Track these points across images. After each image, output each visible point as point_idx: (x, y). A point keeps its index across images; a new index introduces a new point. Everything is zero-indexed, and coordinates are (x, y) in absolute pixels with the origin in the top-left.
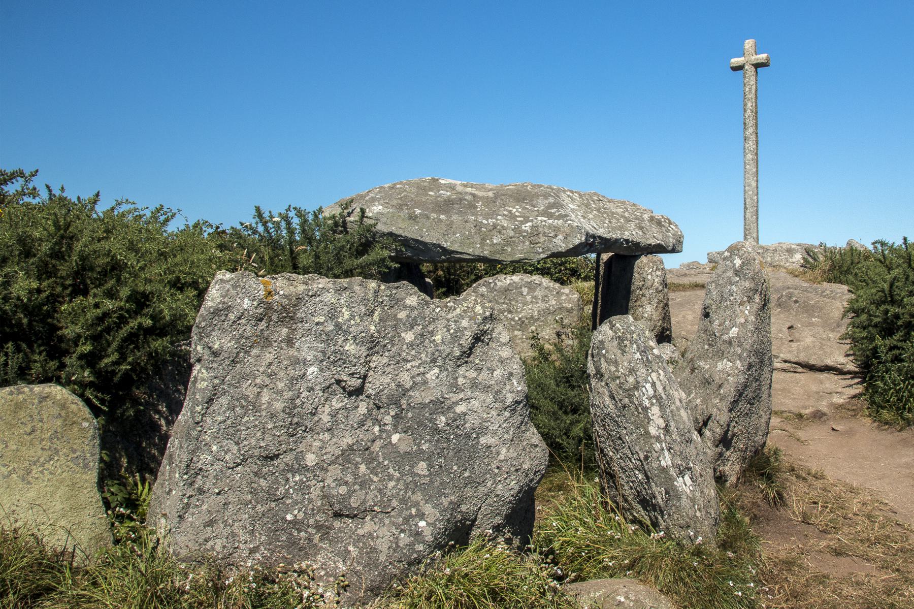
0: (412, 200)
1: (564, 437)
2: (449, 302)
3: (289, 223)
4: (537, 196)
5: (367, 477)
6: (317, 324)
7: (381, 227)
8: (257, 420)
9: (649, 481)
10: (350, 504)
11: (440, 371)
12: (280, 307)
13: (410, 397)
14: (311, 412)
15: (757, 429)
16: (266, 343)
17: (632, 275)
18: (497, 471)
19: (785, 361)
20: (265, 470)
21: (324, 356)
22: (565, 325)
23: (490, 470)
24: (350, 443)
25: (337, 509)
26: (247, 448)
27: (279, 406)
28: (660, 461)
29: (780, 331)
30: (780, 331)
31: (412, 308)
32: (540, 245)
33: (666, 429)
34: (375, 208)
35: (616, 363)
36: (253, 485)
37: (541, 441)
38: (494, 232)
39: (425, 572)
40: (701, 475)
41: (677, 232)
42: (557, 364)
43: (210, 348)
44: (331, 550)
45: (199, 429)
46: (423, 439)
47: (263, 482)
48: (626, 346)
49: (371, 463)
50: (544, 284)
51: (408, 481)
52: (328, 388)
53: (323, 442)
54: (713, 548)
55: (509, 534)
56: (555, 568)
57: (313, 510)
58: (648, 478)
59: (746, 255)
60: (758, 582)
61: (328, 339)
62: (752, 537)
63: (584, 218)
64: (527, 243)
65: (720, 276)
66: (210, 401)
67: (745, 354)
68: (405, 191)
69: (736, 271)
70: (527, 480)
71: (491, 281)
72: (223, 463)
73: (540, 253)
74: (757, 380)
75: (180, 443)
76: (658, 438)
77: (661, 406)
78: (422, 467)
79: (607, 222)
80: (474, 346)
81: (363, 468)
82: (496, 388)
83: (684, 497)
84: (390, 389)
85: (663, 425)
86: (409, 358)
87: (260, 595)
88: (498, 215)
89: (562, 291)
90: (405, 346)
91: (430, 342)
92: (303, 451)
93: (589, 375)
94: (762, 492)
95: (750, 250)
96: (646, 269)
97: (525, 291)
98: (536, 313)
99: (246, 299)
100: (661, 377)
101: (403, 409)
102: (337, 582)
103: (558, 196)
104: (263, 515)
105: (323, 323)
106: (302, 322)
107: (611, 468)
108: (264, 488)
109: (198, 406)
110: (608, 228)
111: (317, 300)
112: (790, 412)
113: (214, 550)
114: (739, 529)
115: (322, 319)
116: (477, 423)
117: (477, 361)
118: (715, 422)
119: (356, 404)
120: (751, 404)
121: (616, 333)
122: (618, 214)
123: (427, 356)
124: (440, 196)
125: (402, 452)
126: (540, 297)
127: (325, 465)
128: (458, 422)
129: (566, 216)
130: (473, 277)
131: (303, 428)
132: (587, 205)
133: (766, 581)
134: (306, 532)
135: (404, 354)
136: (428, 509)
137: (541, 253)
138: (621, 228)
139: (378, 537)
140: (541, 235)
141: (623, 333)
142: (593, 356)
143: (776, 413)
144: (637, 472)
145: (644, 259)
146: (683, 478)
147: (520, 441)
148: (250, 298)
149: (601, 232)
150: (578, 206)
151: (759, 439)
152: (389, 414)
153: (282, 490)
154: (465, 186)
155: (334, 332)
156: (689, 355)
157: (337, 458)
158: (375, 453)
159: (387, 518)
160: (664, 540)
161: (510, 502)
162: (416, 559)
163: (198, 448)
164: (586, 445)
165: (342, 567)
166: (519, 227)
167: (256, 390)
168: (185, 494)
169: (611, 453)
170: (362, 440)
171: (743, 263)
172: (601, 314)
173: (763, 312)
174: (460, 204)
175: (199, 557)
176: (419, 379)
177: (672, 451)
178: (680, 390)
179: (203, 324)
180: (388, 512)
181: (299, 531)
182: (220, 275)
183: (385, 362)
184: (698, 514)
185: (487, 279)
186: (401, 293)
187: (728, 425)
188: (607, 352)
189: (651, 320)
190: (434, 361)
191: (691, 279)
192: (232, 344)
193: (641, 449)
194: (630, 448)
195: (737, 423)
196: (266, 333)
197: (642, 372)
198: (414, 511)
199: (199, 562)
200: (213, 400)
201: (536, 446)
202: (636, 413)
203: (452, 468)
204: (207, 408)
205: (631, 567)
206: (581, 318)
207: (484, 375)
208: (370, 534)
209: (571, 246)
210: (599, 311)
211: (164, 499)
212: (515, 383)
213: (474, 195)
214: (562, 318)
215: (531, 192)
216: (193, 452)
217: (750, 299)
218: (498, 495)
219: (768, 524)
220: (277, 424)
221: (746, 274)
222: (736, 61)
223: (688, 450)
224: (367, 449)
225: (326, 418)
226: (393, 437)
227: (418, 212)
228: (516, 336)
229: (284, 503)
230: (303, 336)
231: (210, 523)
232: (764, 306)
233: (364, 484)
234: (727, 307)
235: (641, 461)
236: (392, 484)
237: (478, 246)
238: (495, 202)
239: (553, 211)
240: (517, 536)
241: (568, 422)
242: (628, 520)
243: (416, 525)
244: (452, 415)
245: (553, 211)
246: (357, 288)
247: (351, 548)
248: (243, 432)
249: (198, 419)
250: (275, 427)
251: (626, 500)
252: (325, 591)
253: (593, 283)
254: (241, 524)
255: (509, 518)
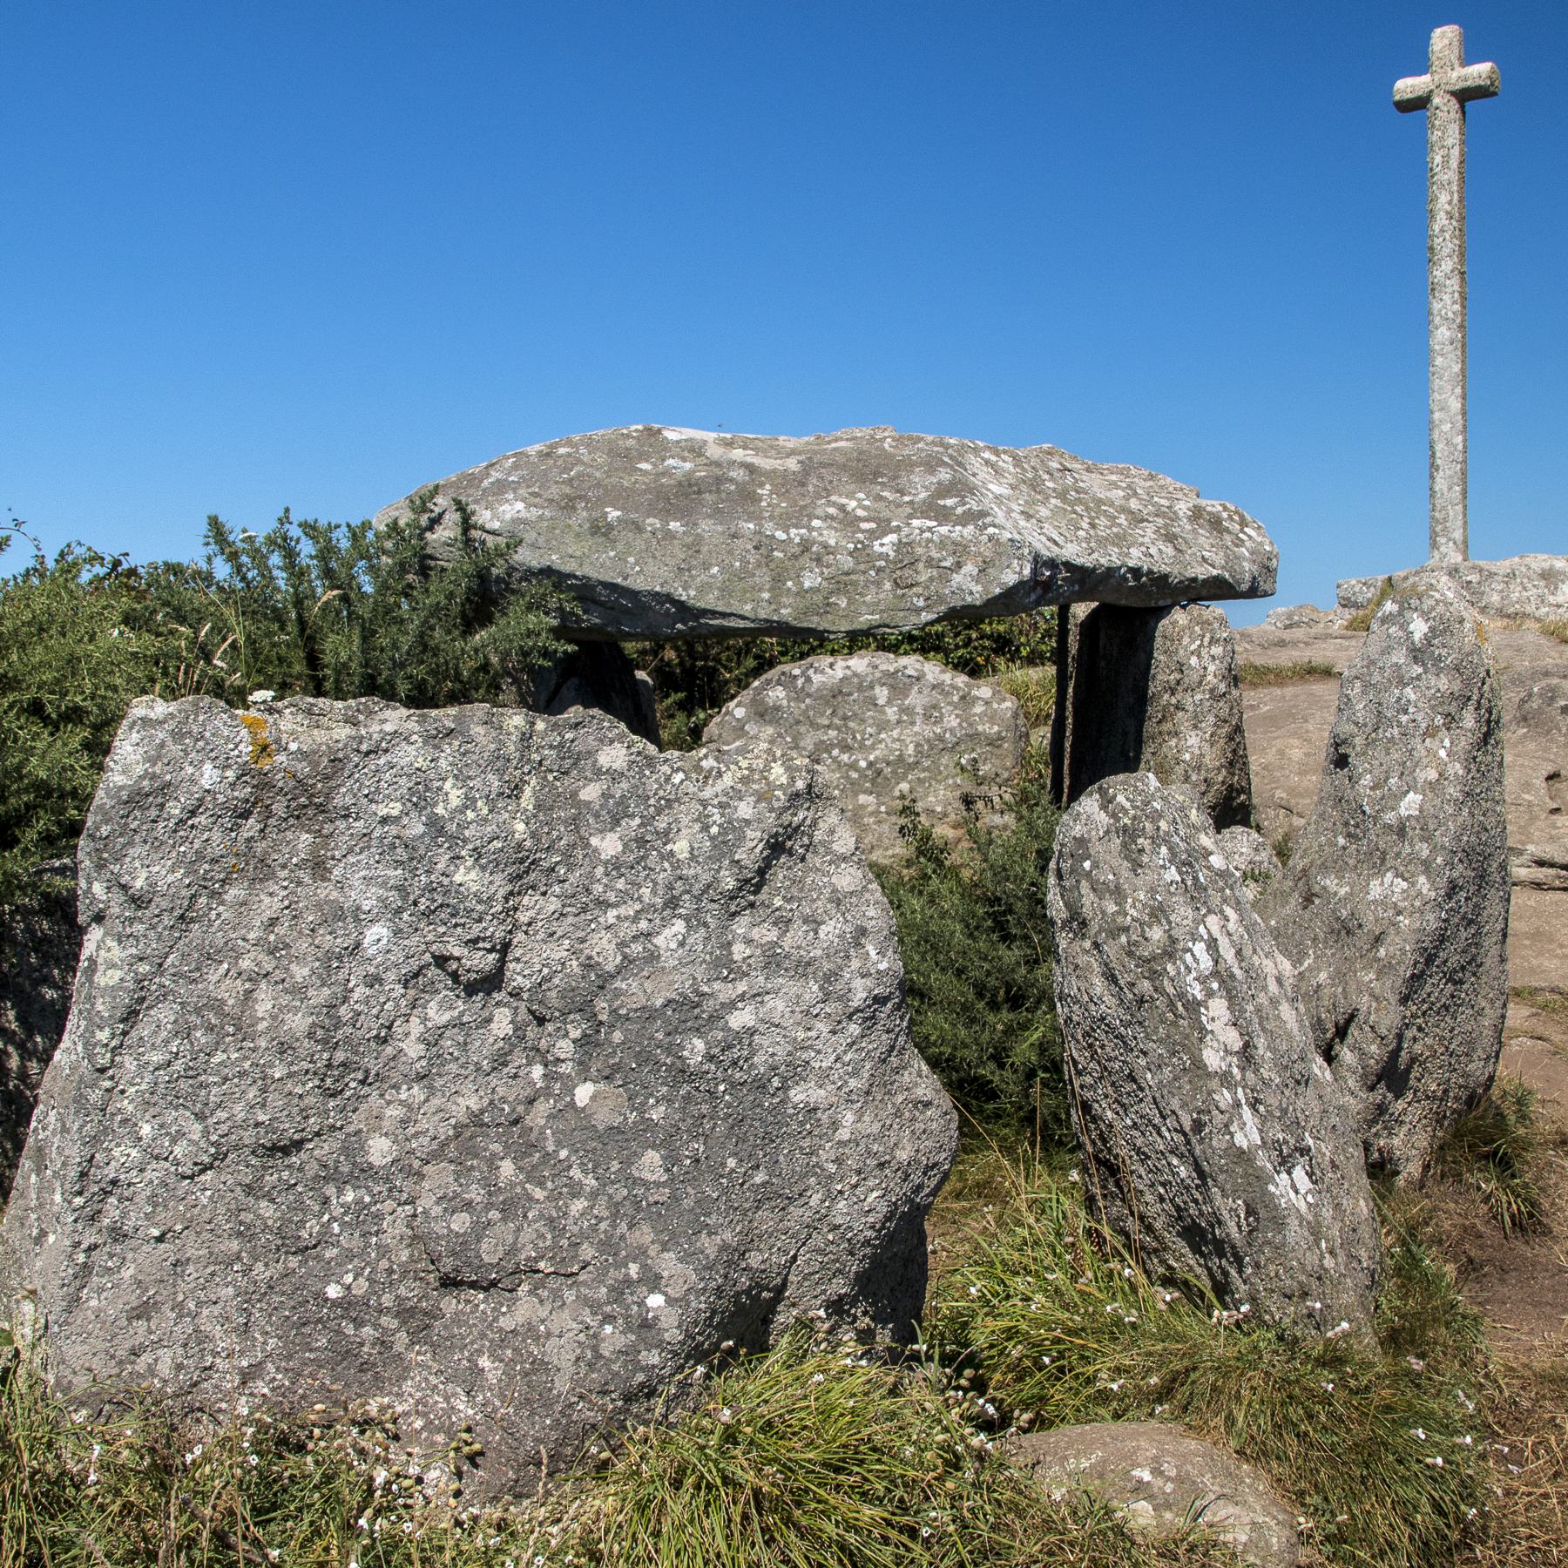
0: (598, 485)
1: (992, 1065)
2: (706, 756)
3: (290, 555)
4: (908, 465)
5: (518, 1189)
6: (384, 820)
7: (525, 557)
8: (246, 1058)
9: (1205, 1184)
10: (479, 1257)
11: (689, 927)
12: (292, 783)
13: (618, 993)
14: (377, 1037)
15: (1471, 1044)
16: (262, 871)
17: (1150, 656)
18: (832, 1168)
19: (1541, 863)
20: (270, 1179)
21: (405, 898)
22: (984, 778)
23: (817, 1165)
24: (475, 1108)
25: (448, 1268)
26: (224, 1128)
27: (298, 1023)
28: (1232, 1135)
29: (1527, 786)
30: (1527, 786)
31: (615, 776)
32: (919, 590)
33: (1246, 1054)
34: (506, 507)
35: (1118, 893)
36: (243, 1216)
37: (937, 1091)
38: (805, 560)
39: (666, 1416)
40: (1334, 1166)
41: (1261, 544)
42: (966, 874)
43: (124, 888)
44: (436, 1367)
45: (108, 1084)
46: (651, 1095)
47: (266, 1209)
48: (1141, 851)
49: (526, 1154)
50: (930, 677)
51: (618, 1198)
52: (416, 975)
53: (409, 1107)
54: (1367, 1344)
55: (867, 1320)
56: (981, 1401)
57: (390, 1271)
58: (1202, 1175)
59: (1440, 609)
60: (1485, 1431)
61: (411, 856)
62: (1464, 1317)
63: (1028, 516)
64: (888, 586)
65: (1373, 662)
66: (131, 1016)
67: (1439, 860)
68: (579, 461)
69: (1414, 650)
70: (907, 1187)
71: (797, 672)
72: (167, 1165)
73: (918, 611)
74: (1471, 922)
75: (61, 1119)
76: (1225, 1078)
77: (1231, 998)
78: (651, 1164)
79: (1085, 526)
80: (768, 866)
81: (507, 1168)
82: (827, 966)
83: (1293, 1222)
84: (566, 975)
85: (1237, 1044)
86: (612, 898)
87: (266, 1480)
88: (811, 517)
89: (975, 692)
90: (600, 870)
91: (662, 857)
92: (360, 1131)
93: (1052, 923)
94: (1487, 1199)
95: (1450, 595)
96: (1186, 640)
97: (882, 694)
98: (911, 749)
99: (208, 766)
100: (1231, 926)
101: (601, 1023)
102: (454, 1444)
103: (960, 464)
104: (271, 1288)
105: (398, 818)
106: (346, 817)
107: (1110, 1150)
108: (270, 1222)
109: (101, 1028)
110: (1087, 539)
111: (382, 761)
112: (1552, 991)
113: (154, 1376)
114: (1430, 1298)
115: (395, 809)
116: (781, 1052)
117: (778, 902)
118: (1367, 1029)
119: (485, 1014)
120: (1455, 983)
121: (1118, 819)
122: (1112, 505)
123: (654, 892)
124: (667, 473)
125: (600, 1128)
126: (919, 710)
127: (416, 1164)
128: (735, 1052)
129: (983, 514)
130: (750, 663)
131: (360, 1076)
132: (1035, 485)
133: (1503, 1426)
134: (376, 1326)
135: (598, 889)
136: (668, 1263)
137: (922, 609)
138: (1120, 540)
139: (549, 1335)
140: (921, 566)
141: (1134, 818)
142: (1060, 876)
143: (1518, 994)
144: (1175, 1162)
145: (1179, 617)
146: (1289, 1173)
147: (889, 1092)
148: (217, 763)
149: (1072, 552)
150: (1013, 487)
151: (1476, 1068)
152: (566, 1035)
153: (313, 1227)
154: (729, 444)
155: (427, 840)
156: (1296, 861)
157: (443, 1145)
158: (536, 1131)
159: (570, 1287)
160: (1245, 1327)
161: (867, 1243)
162: (642, 1385)
163: (105, 1131)
164: (1044, 1084)
165: (464, 1409)
166: (865, 547)
167: (241, 986)
168: (79, 1243)
169: (1109, 1114)
170: (503, 1100)
171: (1432, 629)
172: (1074, 733)
173: (1486, 753)
174: (718, 491)
175: (119, 1391)
176: (636, 948)
177: (1261, 1108)
178: (1277, 954)
179: (105, 830)
180: (573, 1274)
181: (358, 1323)
182: (140, 708)
183: (552, 908)
184: (1329, 1262)
185: (786, 668)
186: (585, 739)
187: (1400, 1037)
188: (1095, 865)
189: (1199, 768)
190: (672, 903)
191: (1295, 653)
192: (178, 875)
193: (1184, 1105)
194: (1155, 1103)
195: (1420, 1029)
196: (260, 847)
197: (1182, 914)
198: (633, 1270)
199: (119, 1403)
200: (137, 1013)
201: (927, 1105)
202: (1170, 1015)
203: (723, 1165)
204: (125, 1033)
205: (1164, 1393)
206: (1023, 760)
207: (796, 937)
208: (530, 1328)
209: (998, 591)
210: (1067, 745)
211: (27, 1253)
212: (873, 953)
213: (751, 468)
214: (975, 760)
215: (894, 456)
216: (95, 1140)
217: (1451, 720)
218: (837, 1227)
219: (1502, 1281)
220: (296, 1068)
221: (1439, 659)
222: (1407, 86)
223: (1300, 1103)
224: (516, 1122)
225: (413, 1049)
226: (577, 1091)
227: (613, 514)
228: (863, 807)
229: (318, 1258)
230: (350, 851)
231: (143, 1311)
232: (1487, 736)
233: (512, 1207)
234: (1391, 740)
235: (1185, 1134)
236: (578, 1205)
237: (766, 595)
238: (803, 484)
239: (949, 502)
240: (885, 1322)
241: (1000, 1027)
242: (1154, 1277)
243: (641, 1304)
244: (720, 1035)
245: (949, 502)
246: (478, 730)
247: (484, 1362)
248: (215, 1090)
249: (103, 1061)
250: (290, 1075)
251: (1149, 1229)
252: (427, 1468)
253: (1051, 670)
254: (216, 1310)
255: (865, 1283)
